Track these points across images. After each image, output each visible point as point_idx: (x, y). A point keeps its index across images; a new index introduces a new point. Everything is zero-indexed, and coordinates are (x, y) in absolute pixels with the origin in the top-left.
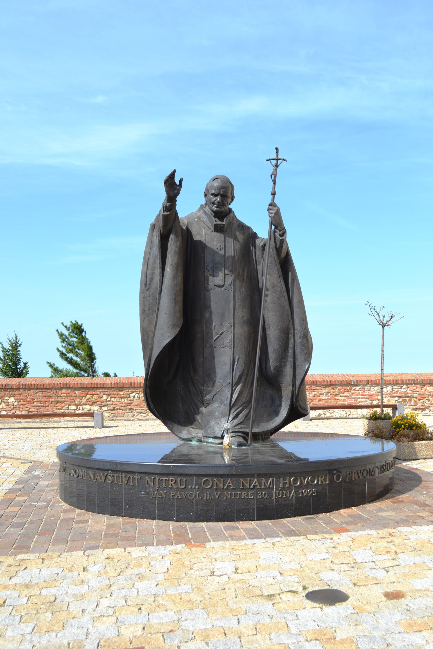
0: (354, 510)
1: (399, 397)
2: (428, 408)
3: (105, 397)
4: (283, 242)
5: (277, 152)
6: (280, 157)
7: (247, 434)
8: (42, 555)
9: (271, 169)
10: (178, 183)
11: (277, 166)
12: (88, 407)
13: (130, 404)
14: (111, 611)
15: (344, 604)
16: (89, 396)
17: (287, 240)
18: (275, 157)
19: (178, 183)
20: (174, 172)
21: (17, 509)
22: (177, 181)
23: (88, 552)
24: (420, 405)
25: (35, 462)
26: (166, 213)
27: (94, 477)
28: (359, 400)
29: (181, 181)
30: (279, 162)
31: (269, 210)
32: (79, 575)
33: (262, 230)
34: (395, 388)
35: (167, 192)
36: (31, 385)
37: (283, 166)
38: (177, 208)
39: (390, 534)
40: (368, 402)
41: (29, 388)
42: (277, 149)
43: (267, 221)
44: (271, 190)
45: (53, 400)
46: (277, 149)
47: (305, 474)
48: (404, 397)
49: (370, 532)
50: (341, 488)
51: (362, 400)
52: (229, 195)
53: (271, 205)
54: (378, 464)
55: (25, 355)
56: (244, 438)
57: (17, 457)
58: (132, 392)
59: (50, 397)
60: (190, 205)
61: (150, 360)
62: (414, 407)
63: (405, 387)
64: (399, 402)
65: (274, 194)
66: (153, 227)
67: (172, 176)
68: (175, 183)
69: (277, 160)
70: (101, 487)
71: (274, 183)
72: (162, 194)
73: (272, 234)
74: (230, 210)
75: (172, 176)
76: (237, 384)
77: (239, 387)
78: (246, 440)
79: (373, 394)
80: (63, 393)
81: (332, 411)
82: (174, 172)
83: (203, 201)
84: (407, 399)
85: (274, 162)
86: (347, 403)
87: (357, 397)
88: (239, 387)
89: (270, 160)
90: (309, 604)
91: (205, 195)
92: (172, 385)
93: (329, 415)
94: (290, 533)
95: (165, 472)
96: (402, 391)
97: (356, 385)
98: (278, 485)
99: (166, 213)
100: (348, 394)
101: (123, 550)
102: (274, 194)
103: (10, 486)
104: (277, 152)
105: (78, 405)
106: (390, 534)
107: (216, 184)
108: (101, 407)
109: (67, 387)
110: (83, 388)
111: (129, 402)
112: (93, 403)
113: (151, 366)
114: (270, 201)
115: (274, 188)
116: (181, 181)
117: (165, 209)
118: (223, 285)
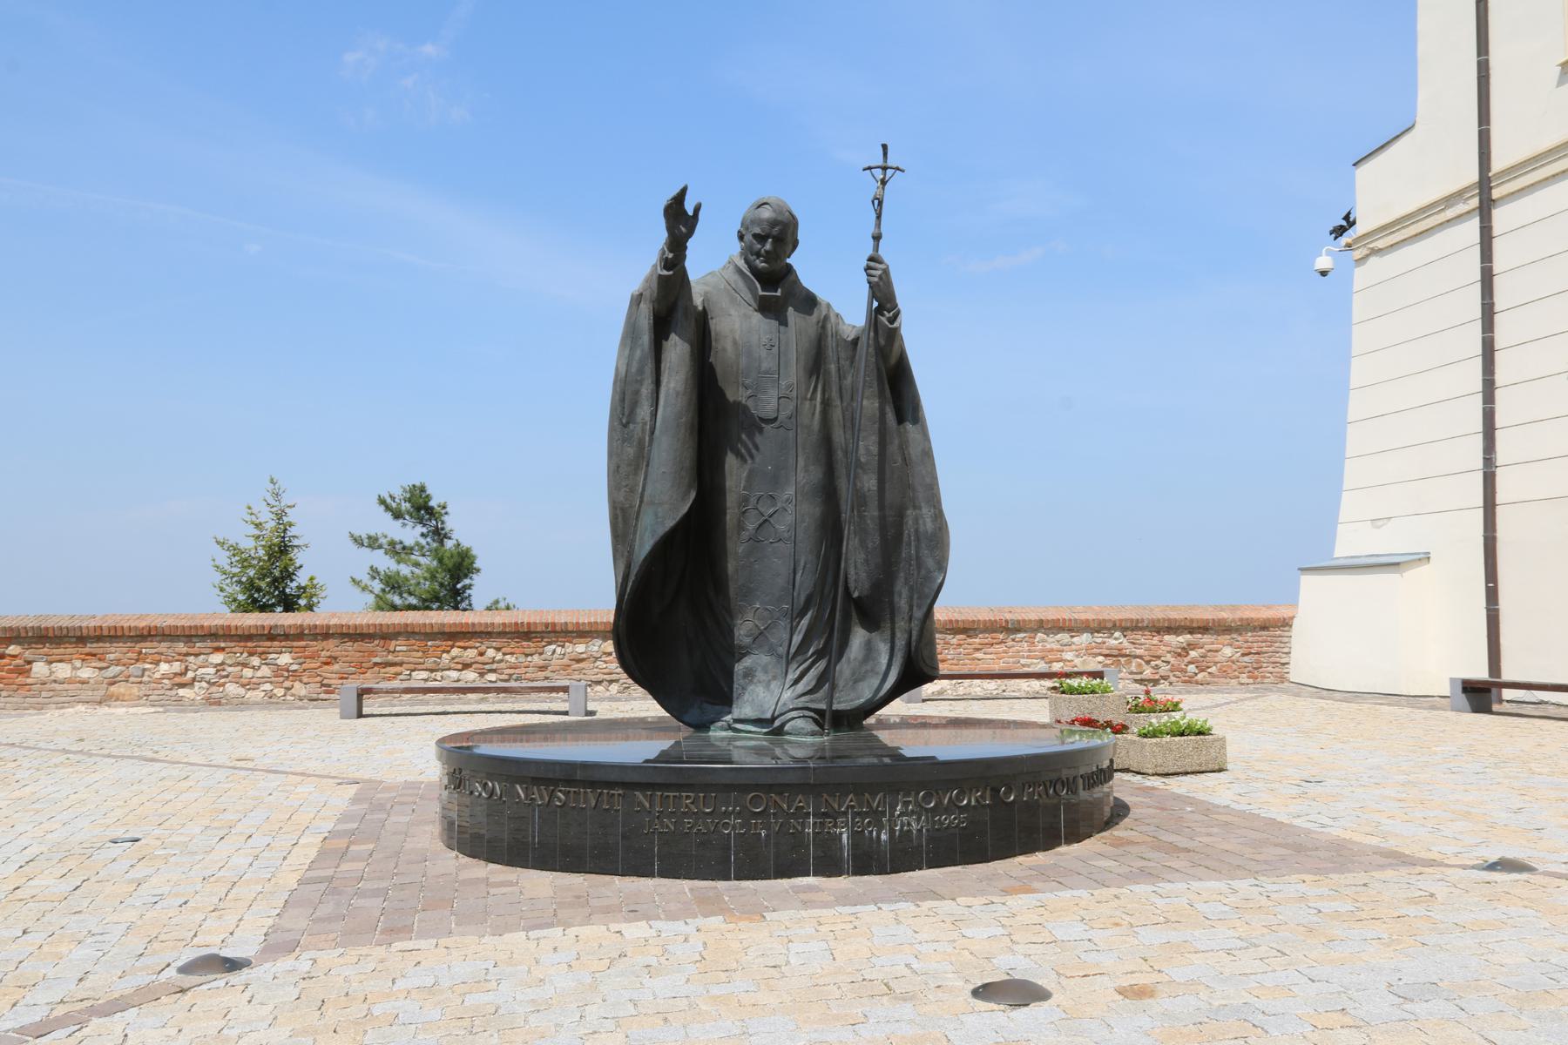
0: (1039, 858)
1: (1106, 656)
2: (1165, 678)
3: (491, 653)
4: (893, 335)
5: (885, 154)
6: (889, 163)
7: (820, 713)
8: (443, 942)
9: (873, 188)
10: (691, 213)
11: (884, 182)
12: (454, 674)
13: (543, 668)
14: (610, 1024)
15: (1045, 1004)
16: (455, 652)
17: (903, 332)
18: (880, 162)
19: (691, 213)
20: (684, 191)
21: (361, 865)
22: (689, 208)
23: (533, 934)
24: (1148, 672)
25: (365, 781)
26: (665, 273)
27: (527, 795)
28: (1023, 661)
29: (697, 209)
30: (889, 172)
31: (868, 268)
32: (529, 971)
33: (850, 308)
34: (1099, 638)
35: (669, 229)
36: (328, 627)
37: (896, 181)
38: (687, 264)
39: (1116, 897)
40: (1041, 667)
41: (325, 634)
42: (885, 147)
43: (865, 290)
44: (871, 229)
45: (377, 660)
46: (885, 147)
47: (948, 785)
48: (1117, 655)
49: (1076, 893)
50: (1025, 809)
51: (1029, 661)
52: (789, 238)
53: (871, 259)
54: (1082, 772)
55: (308, 566)
56: (815, 721)
57: (325, 773)
58: (550, 643)
59: (372, 653)
60: (713, 259)
61: (628, 566)
62: (1138, 677)
63: (1117, 634)
64: (1106, 665)
65: (877, 238)
66: (637, 300)
67: (679, 199)
68: (685, 212)
69: (885, 169)
70: (534, 817)
71: (879, 217)
72: (659, 235)
73: (875, 316)
74: (789, 268)
75: (679, 199)
76: (802, 614)
77: (805, 622)
78: (821, 726)
79: (1052, 650)
80: (400, 645)
81: (967, 682)
82: (684, 191)
83: (735, 248)
84: (1123, 660)
85: (879, 174)
86: (997, 667)
87: (1017, 654)
88: (805, 622)
89: (870, 168)
90: (981, 1005)
91: (741, 237)
92: (672, 618)
93: (961, 691)
94: (919, 895)
95: (673, 780)
96: (1112, 642)
97: (1019, 631)
98: (893, 808)
99: (665, 273)
100: (1002, 648)
101: (604, 928)
102: (877, 238)
103: (330, 826)
104: (885, 154)
105: (432, 671)
106: (1116, 897)
107: (766, 213)
108: (482, 675)
109: (408, 633)
110: (443, 633)
111: (541, 663)
112: (466, 666)
113: (632, 578)
114: (870, 252)
115: (878, 225)
116: (697, 209)
117: (667, 264)
118: (776, 419)
